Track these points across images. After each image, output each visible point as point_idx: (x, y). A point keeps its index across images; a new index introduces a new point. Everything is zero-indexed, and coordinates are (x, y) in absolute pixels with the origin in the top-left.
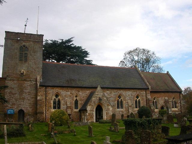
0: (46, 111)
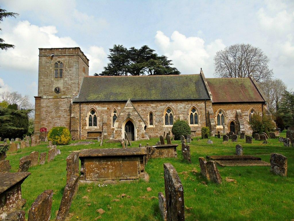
0: (80, 129)
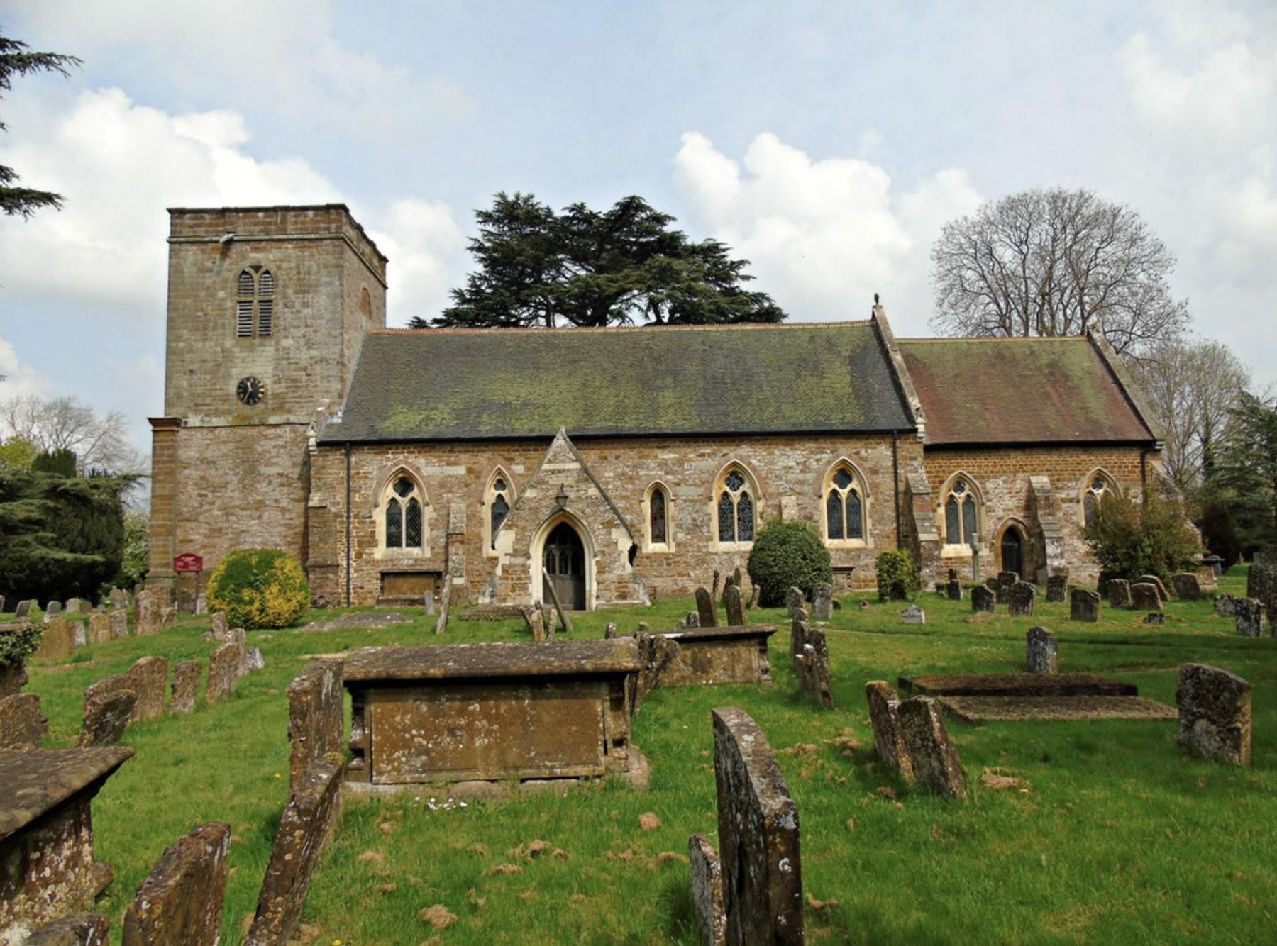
0: (348, 559)
